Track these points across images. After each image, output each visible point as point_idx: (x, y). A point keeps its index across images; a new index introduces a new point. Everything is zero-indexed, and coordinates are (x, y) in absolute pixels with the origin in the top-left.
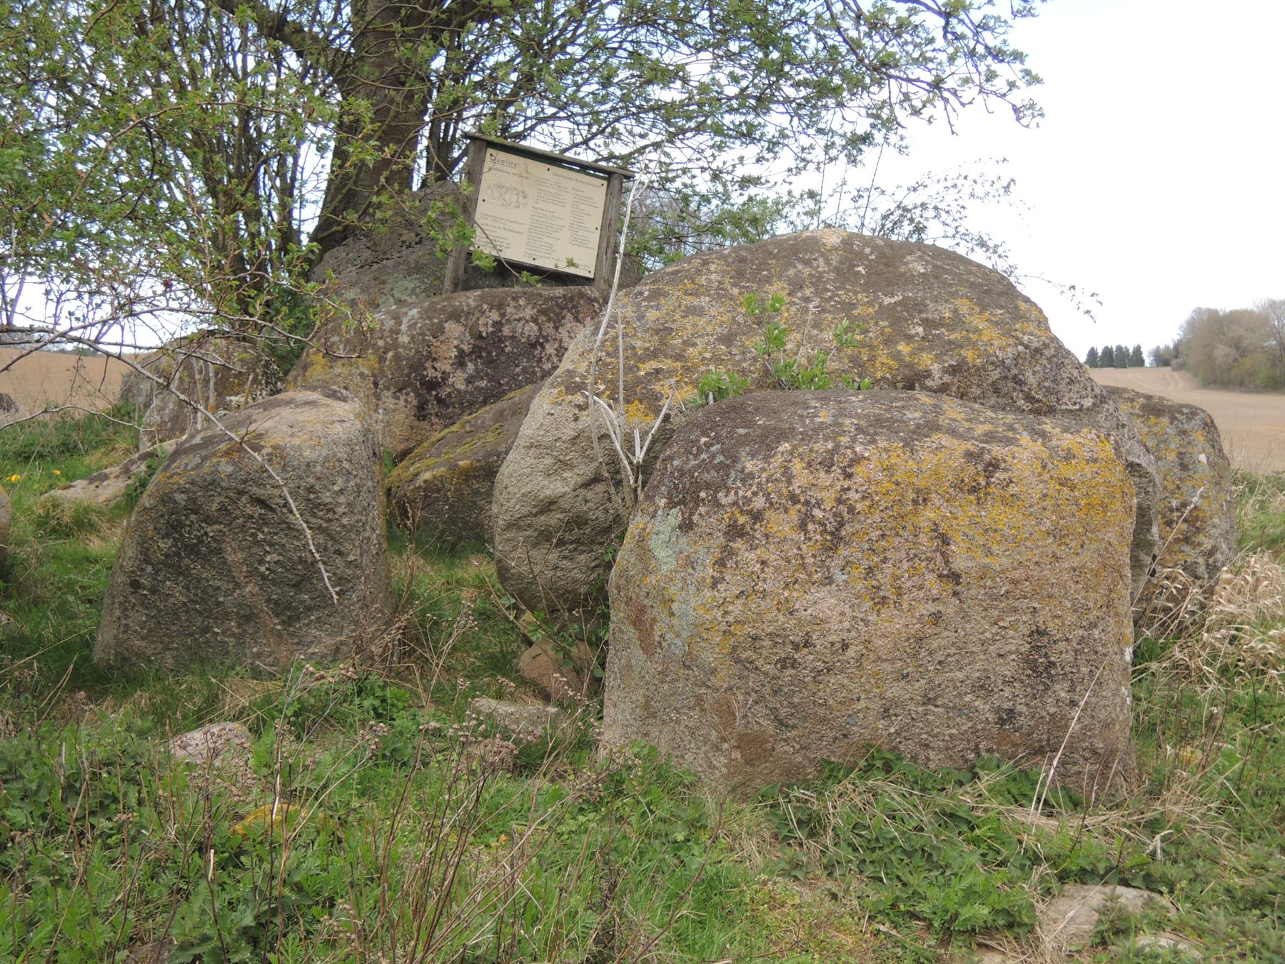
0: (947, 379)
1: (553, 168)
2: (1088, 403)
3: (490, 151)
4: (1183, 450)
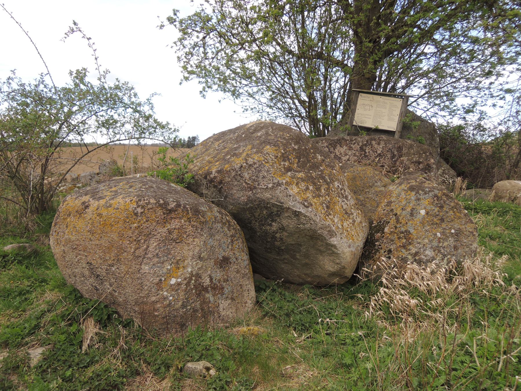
0: (216, 175)
1: (382, 97)
2: (270, 186)
3: (360, 94)
4: (414, 207)
